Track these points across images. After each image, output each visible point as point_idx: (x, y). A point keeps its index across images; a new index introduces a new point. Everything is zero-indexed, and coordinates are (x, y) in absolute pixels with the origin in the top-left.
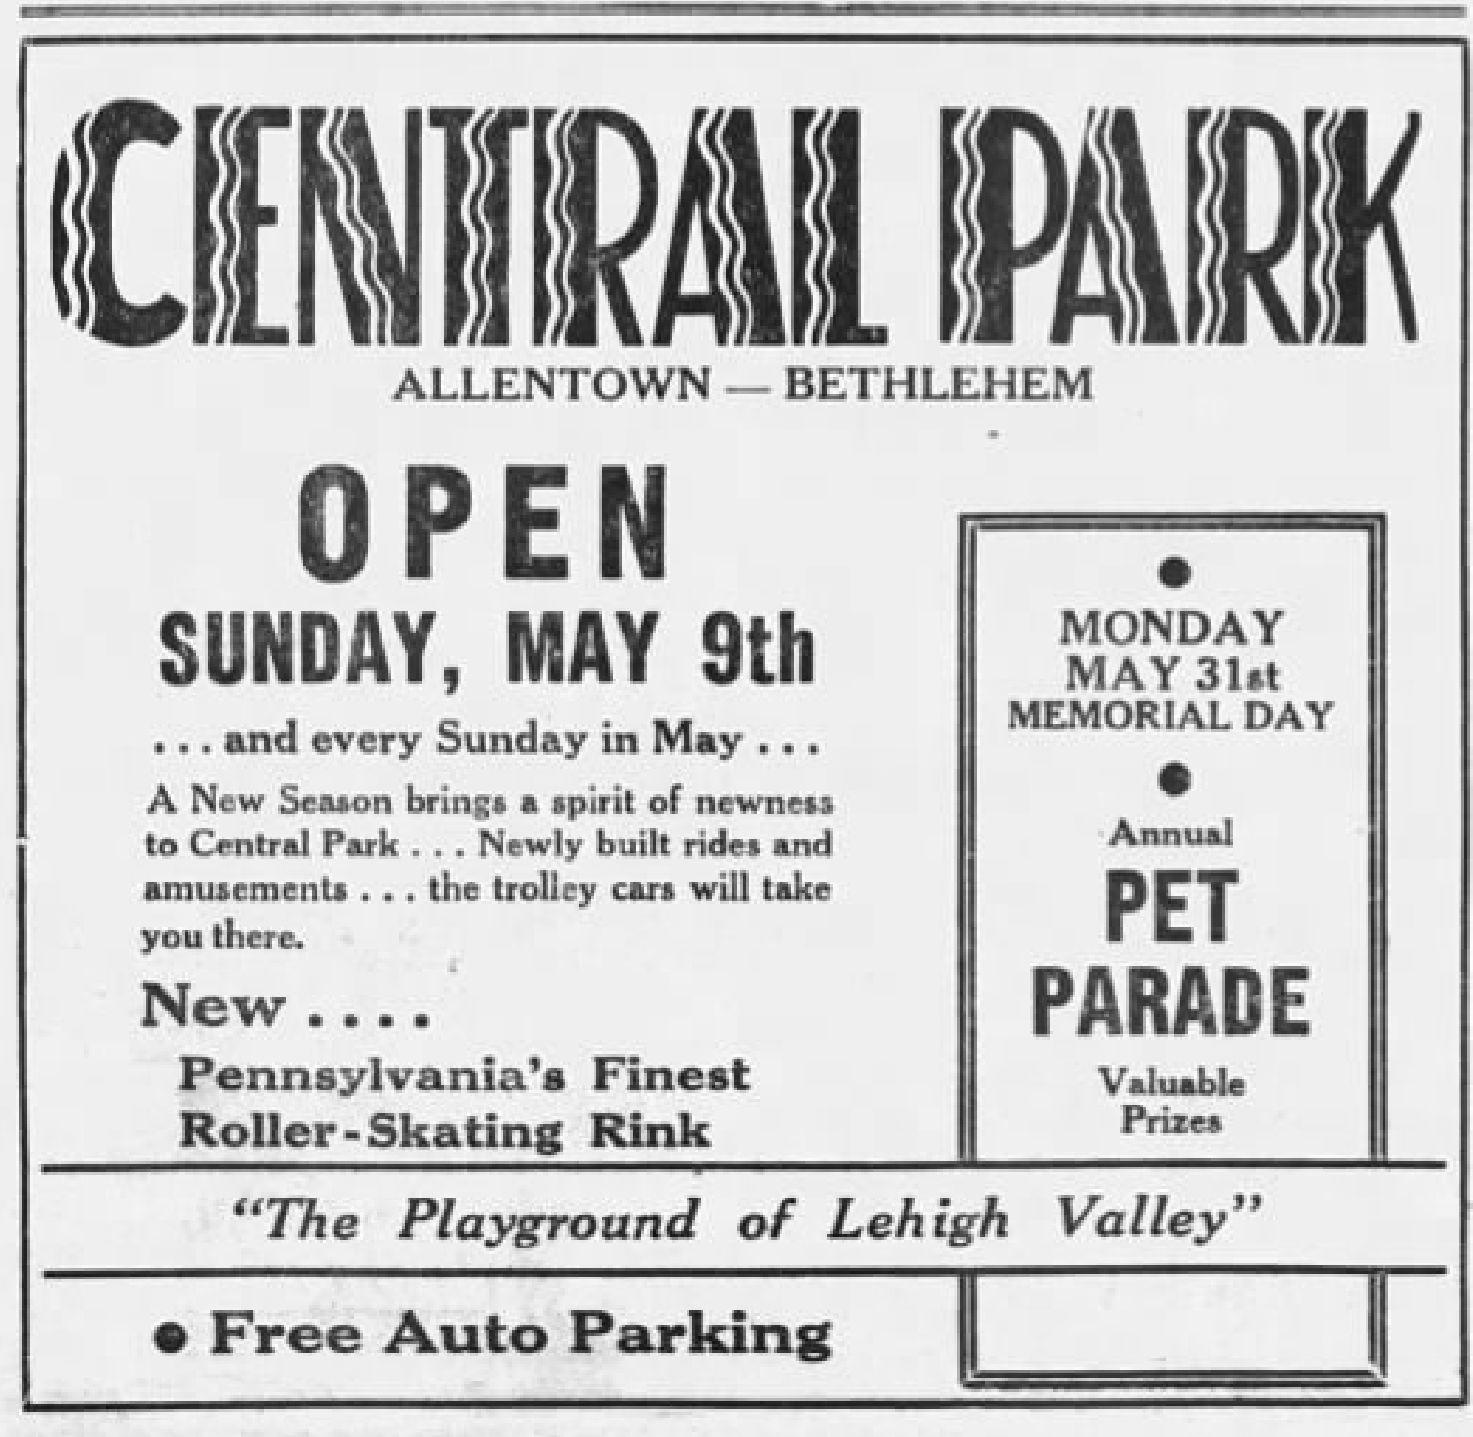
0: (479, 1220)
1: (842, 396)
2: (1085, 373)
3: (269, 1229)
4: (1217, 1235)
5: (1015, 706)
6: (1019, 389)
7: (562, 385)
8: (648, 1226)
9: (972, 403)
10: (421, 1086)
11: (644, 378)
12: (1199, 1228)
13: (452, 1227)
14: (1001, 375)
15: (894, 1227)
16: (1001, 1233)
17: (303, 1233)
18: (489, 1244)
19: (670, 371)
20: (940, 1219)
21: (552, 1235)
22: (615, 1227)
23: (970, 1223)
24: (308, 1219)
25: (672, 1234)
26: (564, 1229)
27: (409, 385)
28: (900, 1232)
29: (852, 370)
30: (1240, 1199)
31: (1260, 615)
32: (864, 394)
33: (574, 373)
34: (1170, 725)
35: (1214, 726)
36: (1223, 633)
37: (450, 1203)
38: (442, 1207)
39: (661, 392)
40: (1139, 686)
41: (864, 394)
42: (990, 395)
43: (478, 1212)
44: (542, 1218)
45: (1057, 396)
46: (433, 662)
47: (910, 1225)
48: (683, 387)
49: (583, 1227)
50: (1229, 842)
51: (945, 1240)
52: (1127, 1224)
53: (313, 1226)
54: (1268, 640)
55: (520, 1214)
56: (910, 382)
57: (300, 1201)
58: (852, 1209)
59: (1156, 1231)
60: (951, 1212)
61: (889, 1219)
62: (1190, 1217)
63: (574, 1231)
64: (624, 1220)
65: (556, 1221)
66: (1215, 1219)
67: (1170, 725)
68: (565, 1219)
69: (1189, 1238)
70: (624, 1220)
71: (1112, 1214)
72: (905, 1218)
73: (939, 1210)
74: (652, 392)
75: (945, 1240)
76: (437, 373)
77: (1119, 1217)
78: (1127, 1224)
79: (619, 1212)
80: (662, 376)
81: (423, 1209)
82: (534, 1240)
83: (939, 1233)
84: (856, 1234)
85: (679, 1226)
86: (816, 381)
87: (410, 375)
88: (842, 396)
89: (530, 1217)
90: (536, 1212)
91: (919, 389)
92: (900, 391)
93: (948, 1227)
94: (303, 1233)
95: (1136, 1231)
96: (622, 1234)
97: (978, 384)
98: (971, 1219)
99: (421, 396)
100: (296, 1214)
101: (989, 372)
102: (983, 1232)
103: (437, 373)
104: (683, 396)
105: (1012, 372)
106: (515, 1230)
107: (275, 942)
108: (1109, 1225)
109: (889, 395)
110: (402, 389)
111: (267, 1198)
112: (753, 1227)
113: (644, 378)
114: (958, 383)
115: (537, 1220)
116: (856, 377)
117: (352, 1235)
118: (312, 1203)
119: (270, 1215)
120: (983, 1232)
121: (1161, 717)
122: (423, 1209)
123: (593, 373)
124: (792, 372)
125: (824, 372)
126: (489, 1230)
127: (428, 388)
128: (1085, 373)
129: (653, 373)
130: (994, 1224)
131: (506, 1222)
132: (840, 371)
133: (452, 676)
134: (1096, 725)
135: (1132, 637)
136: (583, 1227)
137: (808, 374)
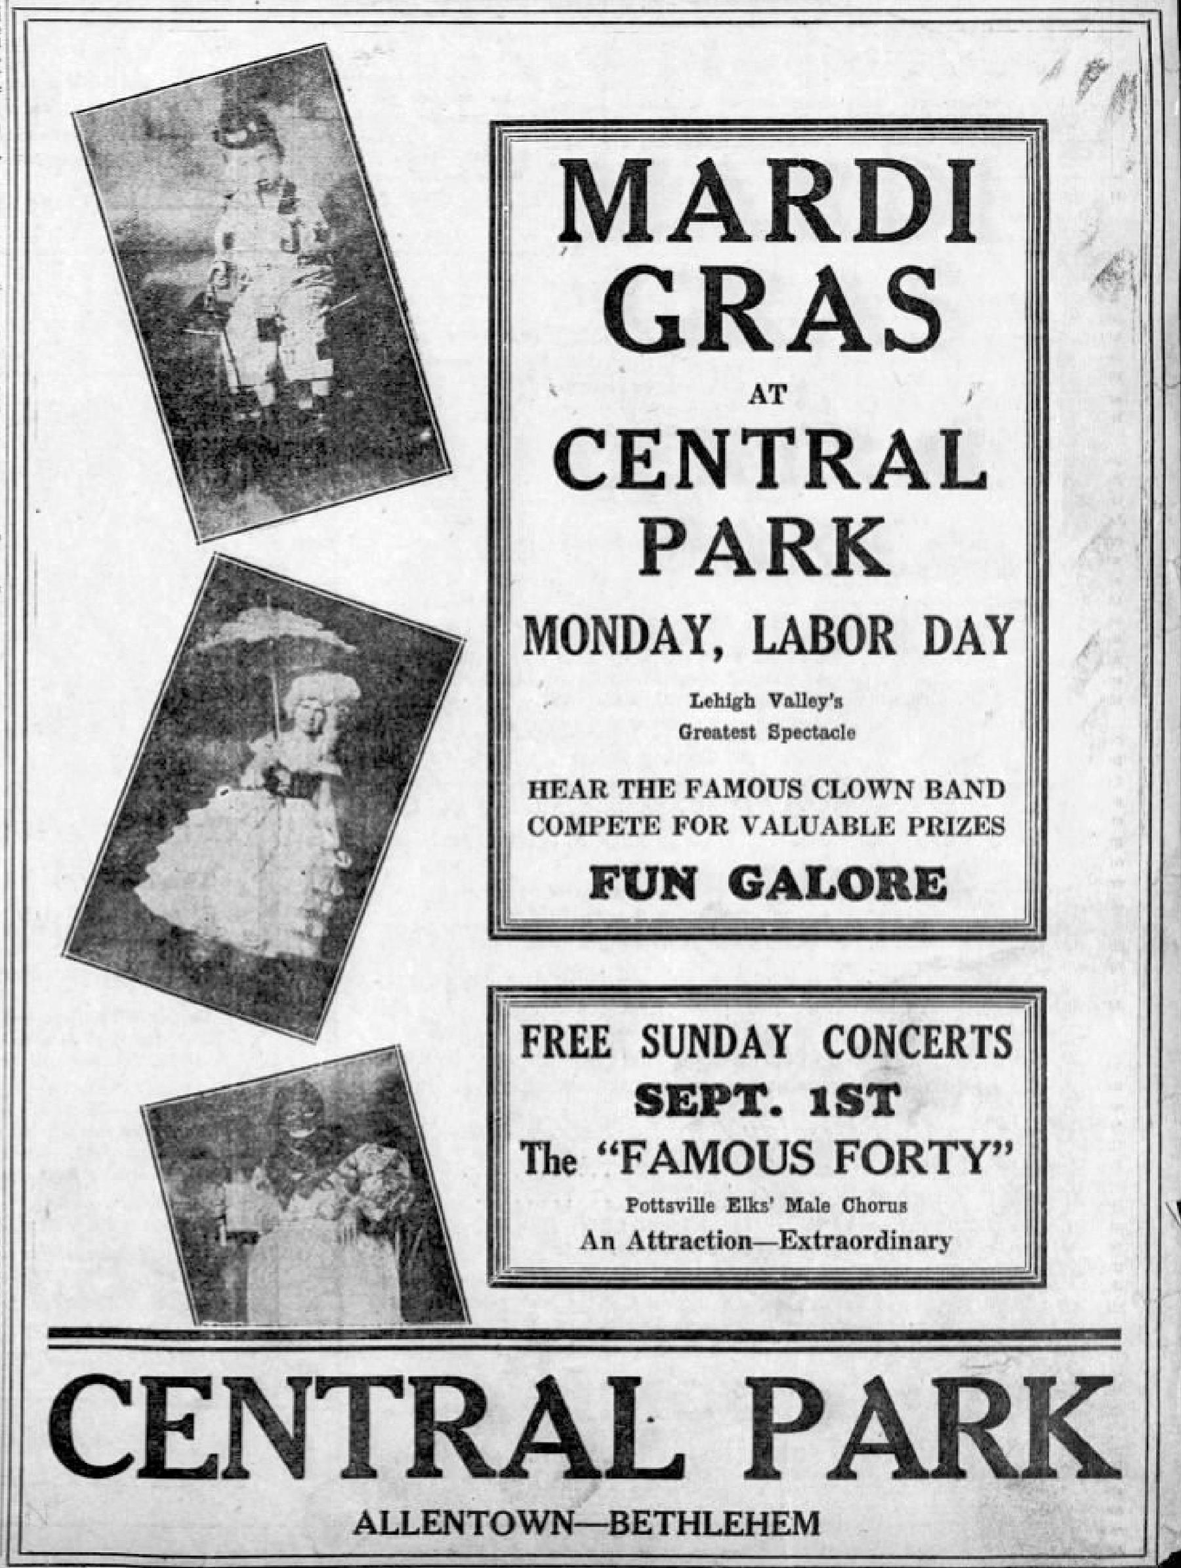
1: (649, 1532)
2: (815, 1515)
6: (770, 1529)
7: (469, 1523)
9: (717, 1538)
10: (682, 1247)
11: (529, 1517)
14: (689, 1517)
19: (547, 1513)
27: (663, 1159)
29: (656, 1513)
32: (665, 1532)
35: (623, 1468)
39: (540, 1529)
40: (735, 233)
41: (665, 1532)
42: (750, 1533)
45: (796, 1533)
46: (708, 644)
48: (555, 1525)
56: (696, 1523)
67: (951, 832)
74: (534, 1529)
76: (951, 437)
86: (631, 1521)
87: (366, 1516)
88: (649, 1532)
91: (702, 1529)
92: (689, 1529)
97: (743, 1524)
99: (373, 1531)
103: (951, 437)
104: (555, 1532)
105: (765, 1514)
107: (872, 1244)
109: (681, 1532)
110: (360, 1526)
113: (529, 1517)
114: (729, 1523)
116: (660, 1517)
123: (492, 1515)
127: (378, 1525)
132: (648, 1513)
133: (719, 652)
134: (552, 650)
137: (626, 1517)
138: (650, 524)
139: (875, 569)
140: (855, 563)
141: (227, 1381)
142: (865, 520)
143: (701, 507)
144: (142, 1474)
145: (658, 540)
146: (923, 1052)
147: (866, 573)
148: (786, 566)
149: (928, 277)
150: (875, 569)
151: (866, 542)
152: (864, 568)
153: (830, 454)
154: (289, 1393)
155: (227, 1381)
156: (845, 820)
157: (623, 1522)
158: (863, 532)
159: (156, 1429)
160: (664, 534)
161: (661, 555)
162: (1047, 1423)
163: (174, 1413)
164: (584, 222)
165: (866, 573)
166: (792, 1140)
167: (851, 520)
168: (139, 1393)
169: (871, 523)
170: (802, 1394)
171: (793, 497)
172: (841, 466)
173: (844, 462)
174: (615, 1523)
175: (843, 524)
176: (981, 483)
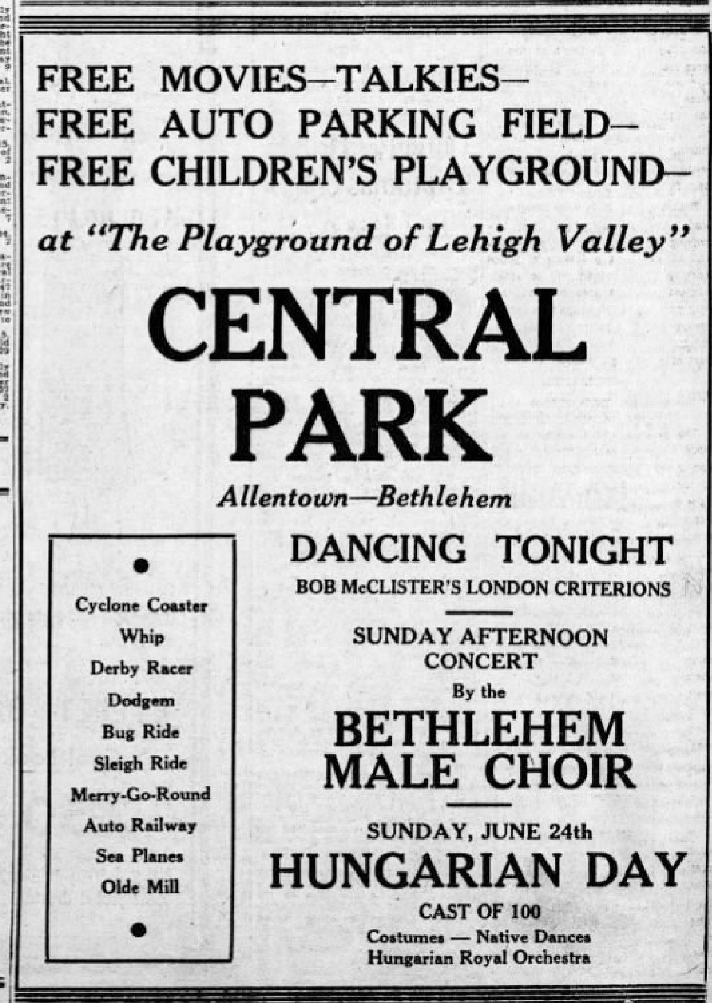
0: (230, 239)
2: (617, 717)
3: (111, 244)
4: (658, 253)
5: (74, 790)
7: (341, 321)
8: (341, 243)
12: (648, 246)
13: (213, 243)
15: (469, 244)
16: (536, 249)
17: (133, 248)
18: (237, 254)
19: (137, 630)
20: (497, 240)
21: (278, 248)
22: (319, 244)
23: (516, 243)
24: (136, 237)
25: (356, 247)
26: (286, 244)
28: (473, 248)
29: (397, 714)
30: (675, 228)
31: (441, 630)
33: (363, 297)
34: (486, 883)
36: (325, 553)
37: (212, 227)
38: (207, 230)
43: (53, 234)
44: (272, 237)
46: (464, 834)
47: (480, 243)
49: (298, 244)
50: (505, 963)
51: (500, 253)
52: (602, 245)
53: (140, 242)
54: (444, 642)
55: (257, 236)
57: (130, 227)
58: (442, 231)
59: (620, 249)
60: (504, 235)
61: (466, 240)
62: (642, 240)
63: (292, 246)
64: (325, 239)
65: (280, 240)
66: (658, 242)
67: (486, 883)
68: (287, 238)
69: (642, 253)
70: (325, 239)
71: (50, 237)
72: (477, 238)
73: (497, 234)
75: (500, 253)
77: (598, 240)
78: (602, 245)
79: (322, 234)
80: (133, 632)
81: (194, 232)
82: (515, 253)
83: (496, 248)
84: (445, 248)
85: (362, 243)
86: (363, 727)
89: (514, 238)
90: (268, 234)
93: (502, 245)
94: (133, 248)
95: (608, 249)
96: (323, 248)
98: (517, 240)
99: (438, 884)
100: (128, 236)
101: (641, 561)
102: (525, 249)
106: (255, 245)
108: (591, 244)
111: (109, 223)
112: (393, 244)
113: (126, 632)
115: (268, 239)
116: (402, 719)
117: (165, 247)
118: (139, 227)
119: (112, 236)
120: (525, 249)
121: (476, 873)
122: (194, 232)
124: (340, 715)
125: (370, 715)
126: (237, 245)
128: (617, 717)
129: (130, 630)
130: (532, 243)
131: (249, 241)
132: (386, 714)
135: (479, 657)
136: (298, 244)
137: (356, 718)
138: (243, 397)
139: (474, 453)
140: (389, 131)
141: (272, 291)
142: (464, 392)
143: (296, 377)
144: (213, 357)
145: (252, 414)
146: (518, 781)
147: (465, 458)
148: (382, 450)
149: (372, 159)
150: (474, 453)
151: (430, 76)
152: (463, 452)
153: (424, 322)
154: (314, 299)
155: (272, 291)
156: (356, 113)
157: (353, 728)
158: (429, 73)
159: (223, 323)
160: (260, 409)
161: (256, 435)
162: (442, 423)
163: (234, 314)
164: (169, 86)
165: (465, 458)
166: (104, 771)
167: (445, 392)
168: (211, 301)
169: (471, 395)
170: (437, 301)
171: (386, 371)
172: (438, 332)
173: (442, 328)
174: (384, 495)
175: (436, 397)
176: (580, 353)
